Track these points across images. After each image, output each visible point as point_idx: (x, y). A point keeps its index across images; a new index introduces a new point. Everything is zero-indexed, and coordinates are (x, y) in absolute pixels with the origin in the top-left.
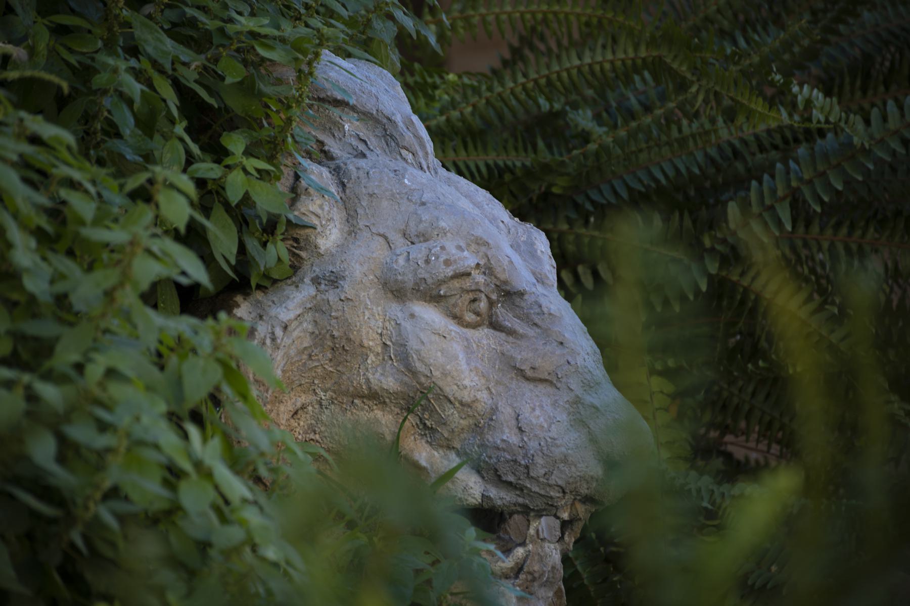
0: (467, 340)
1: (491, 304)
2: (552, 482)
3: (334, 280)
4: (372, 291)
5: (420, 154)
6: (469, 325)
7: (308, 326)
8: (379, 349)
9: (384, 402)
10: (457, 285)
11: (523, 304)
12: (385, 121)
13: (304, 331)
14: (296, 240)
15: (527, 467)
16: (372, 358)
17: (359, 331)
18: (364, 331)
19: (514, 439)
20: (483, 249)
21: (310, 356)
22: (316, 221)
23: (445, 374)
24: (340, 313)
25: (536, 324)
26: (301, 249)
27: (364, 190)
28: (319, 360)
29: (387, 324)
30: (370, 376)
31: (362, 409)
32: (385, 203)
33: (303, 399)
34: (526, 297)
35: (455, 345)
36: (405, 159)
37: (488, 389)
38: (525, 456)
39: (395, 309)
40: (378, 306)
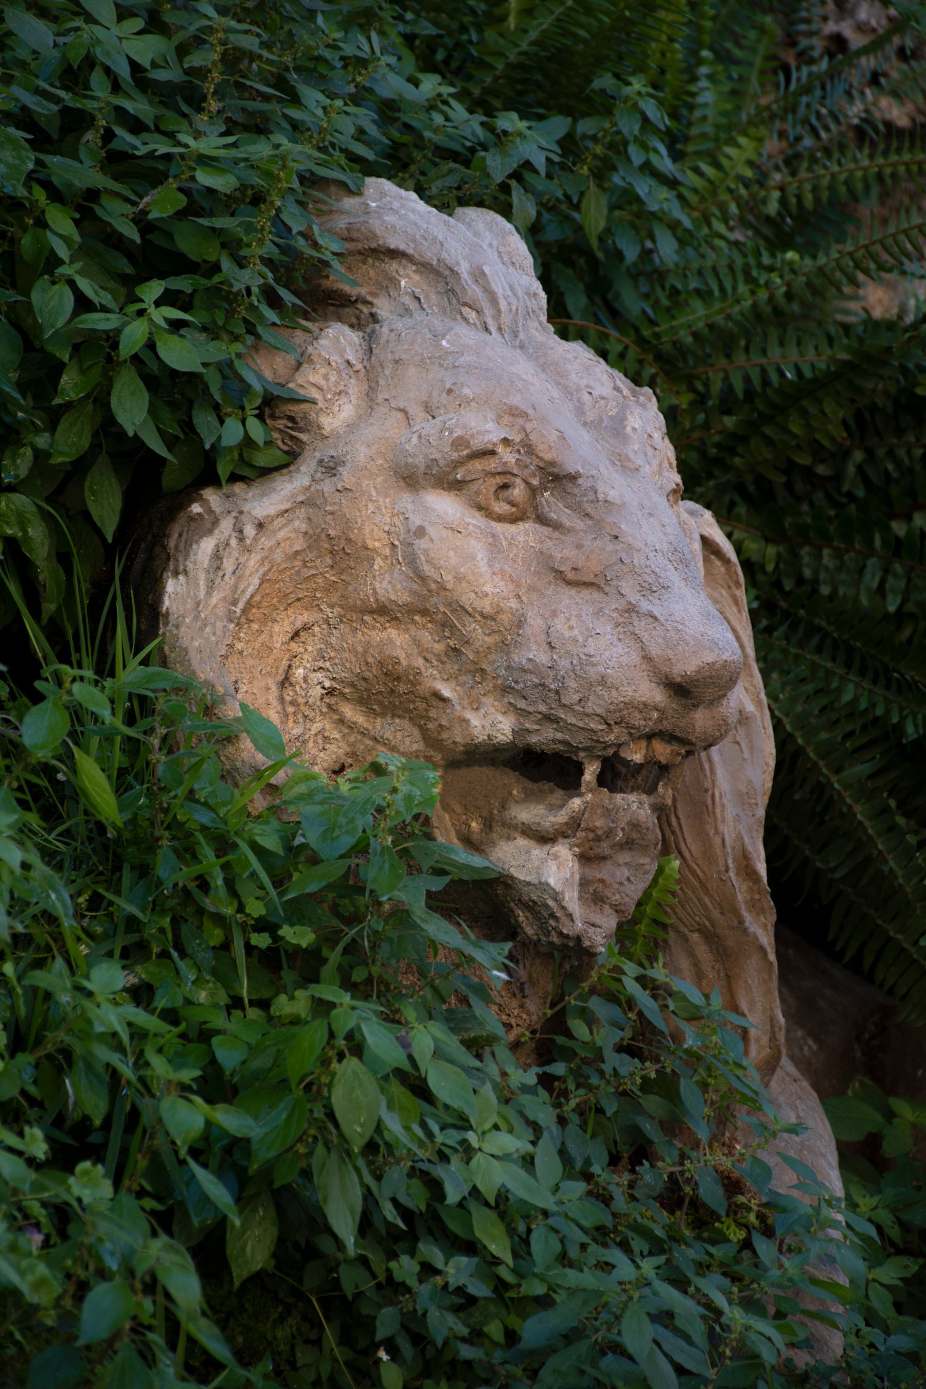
0: (493, 536)
1: (533, 491)
2: (589, 711)
3: (331, 468)
4: (380, 479)
5: (488, 312)
6: (500, 519)
7: (300, 525)
8: (387, 551)
9: (397, 618)
10: (479, 467)
11: (576, 491)
12: (447, 272)
13: (296, 531)
14: (291, 419)
15: (557, 692)
16: (378, 563)
17: (360, 529)
18: (367, 531)
19: (543, 657)
20: (521, 421)
21: (305, 562)
22: (315, 394)
23: (459, 579)
24: (336, 507)
25: (587, 515)
26: (301, 430)
27: (390, 357)
28: (316, 567)
29: (395, 519)
30: (378, 586)
31: (374, 628)
32: (412, 371)
33: (306, 617)
34: (580, 481)
35: (473, 542)
36: (465, 319)
37: (518, 596)
38: (555, 679)
39: (406, 501)
40: (386, 496)
